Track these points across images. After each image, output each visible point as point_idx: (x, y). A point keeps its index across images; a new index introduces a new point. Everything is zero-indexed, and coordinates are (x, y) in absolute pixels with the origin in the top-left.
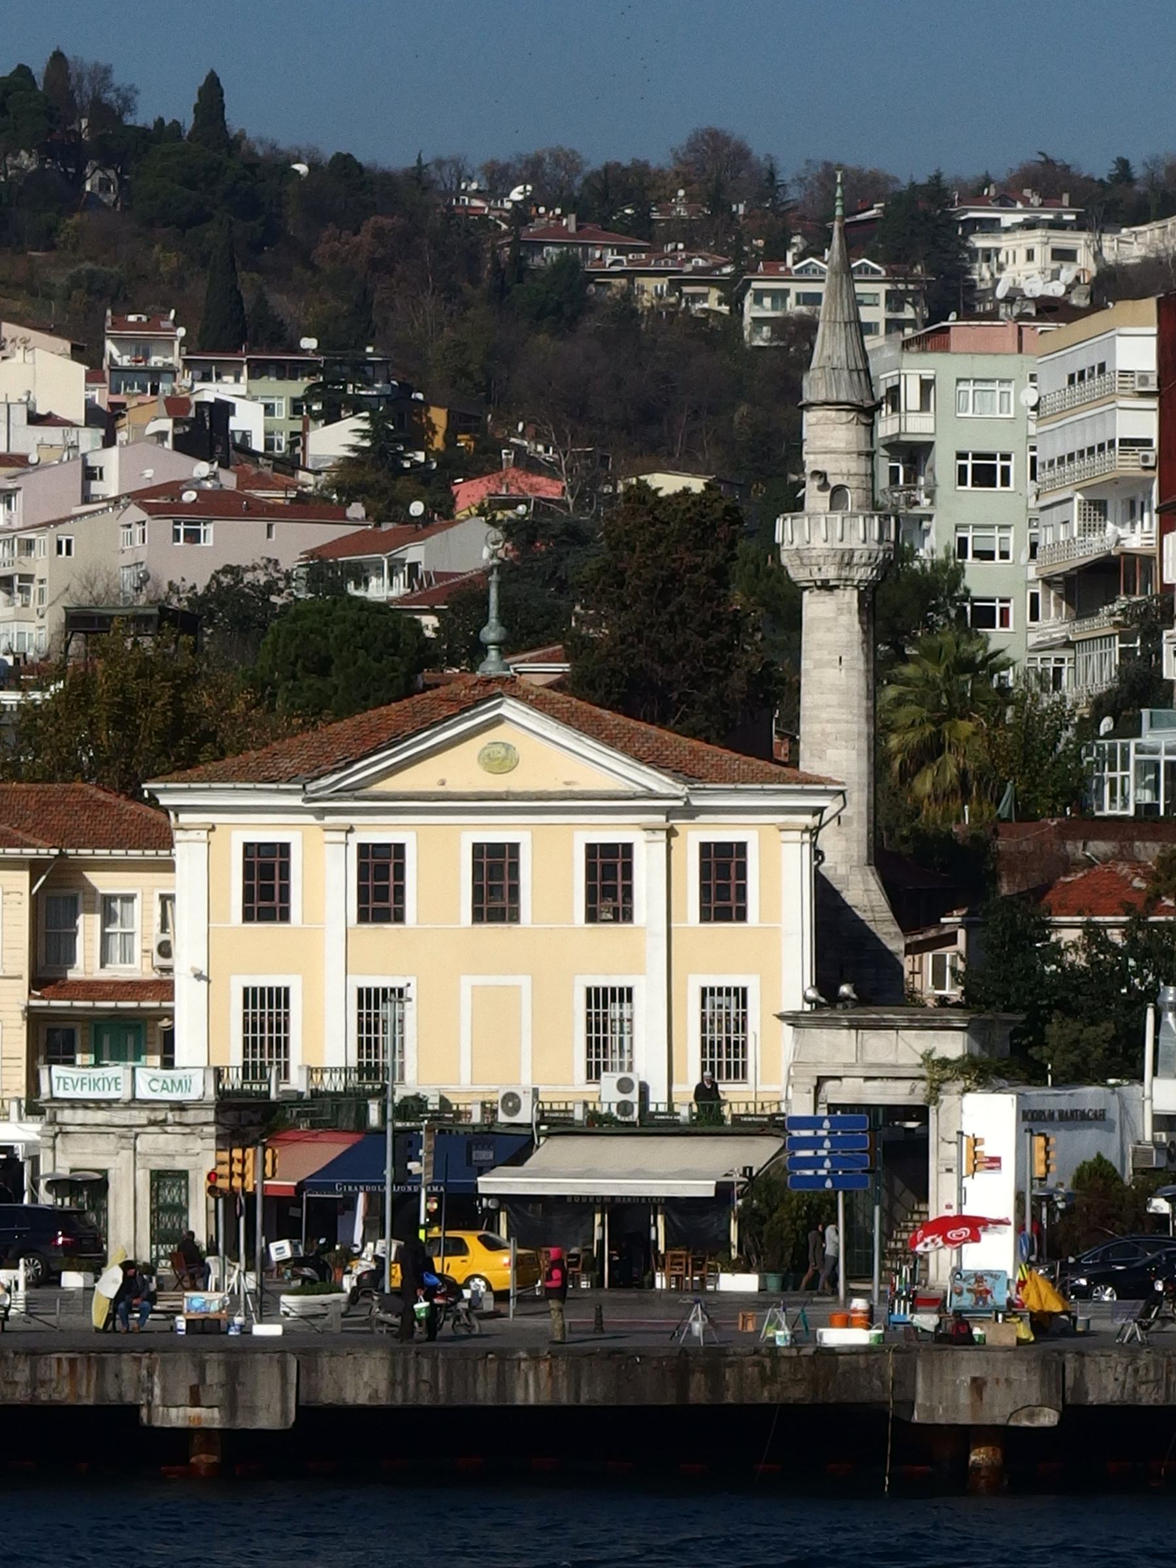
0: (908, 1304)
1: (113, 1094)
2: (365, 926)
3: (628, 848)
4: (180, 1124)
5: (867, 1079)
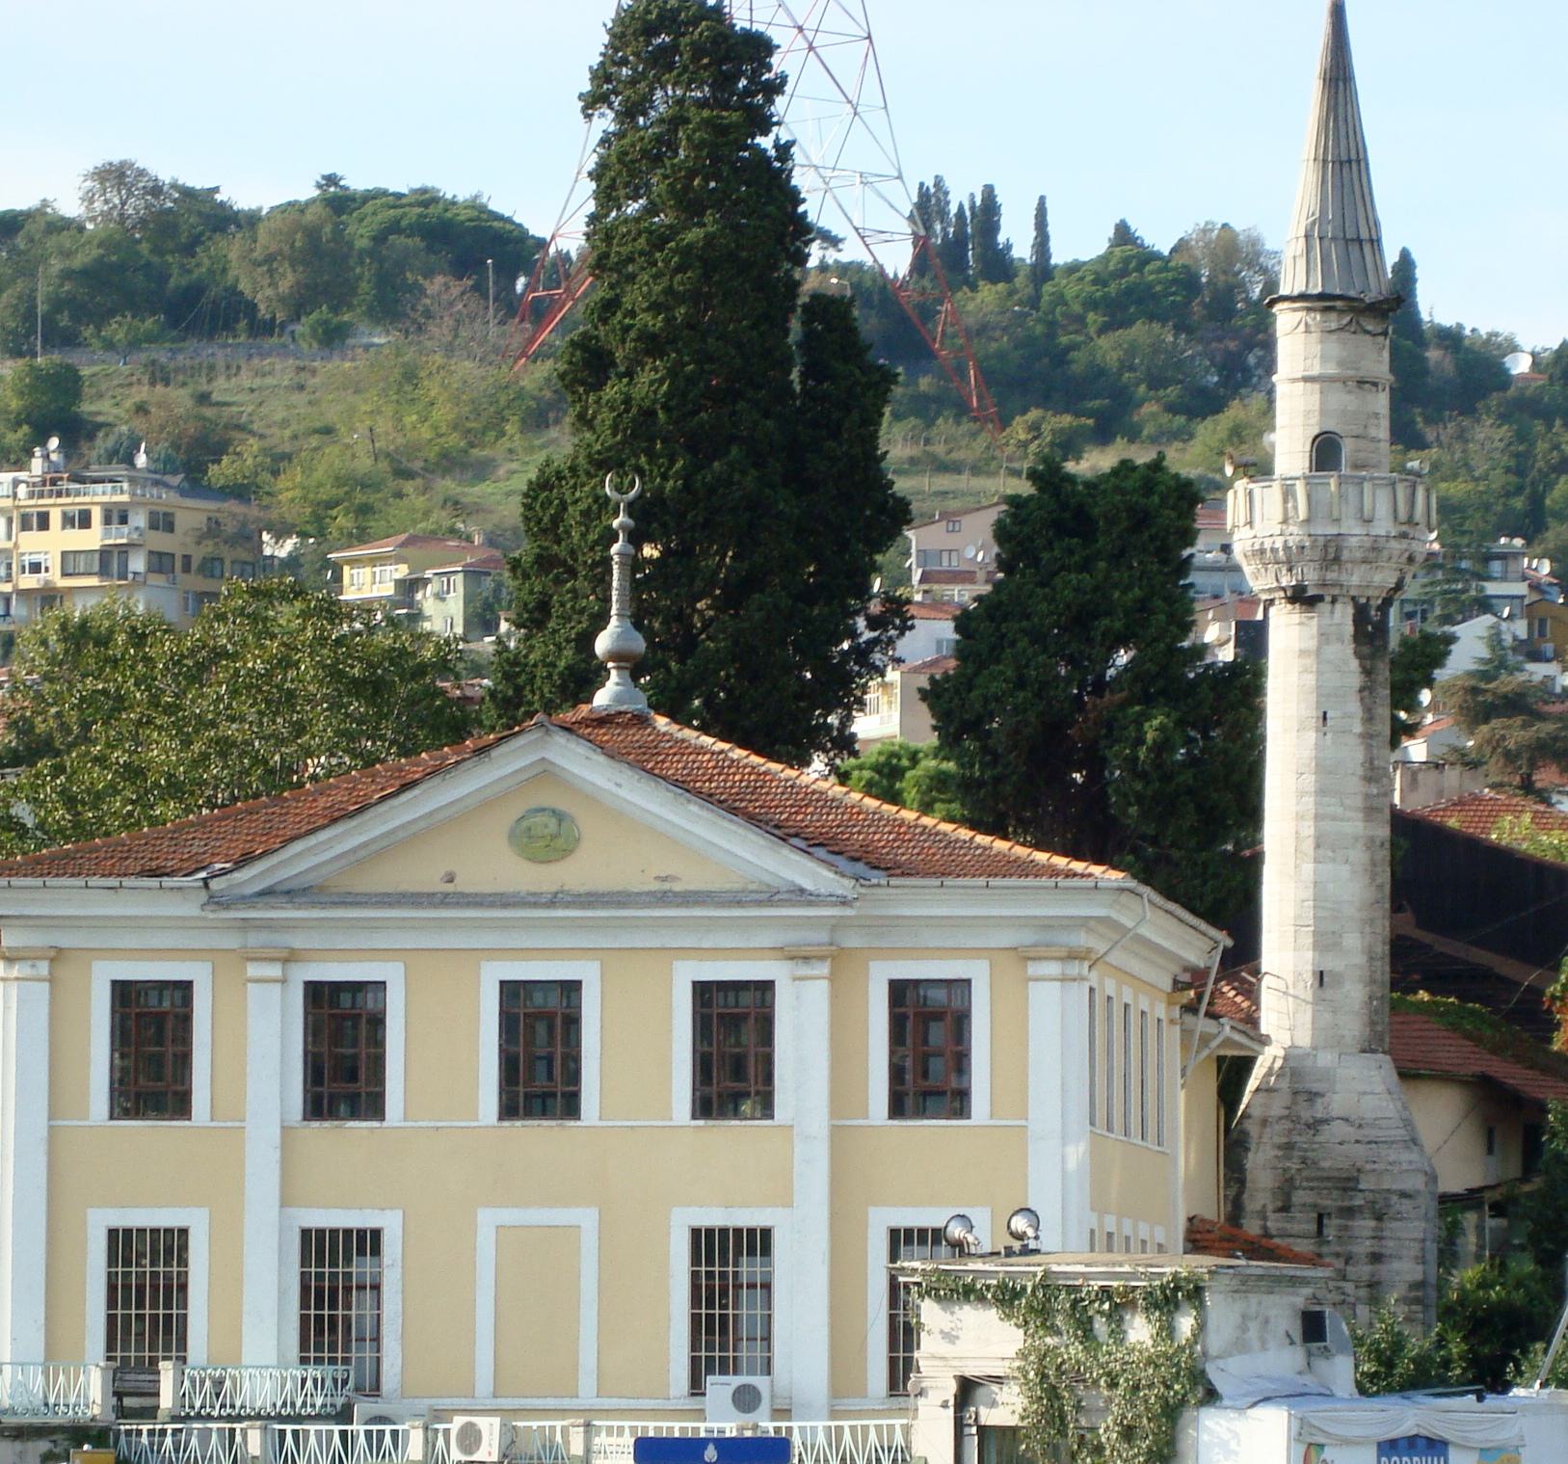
2: (315, 1124)
3: (766, 987)
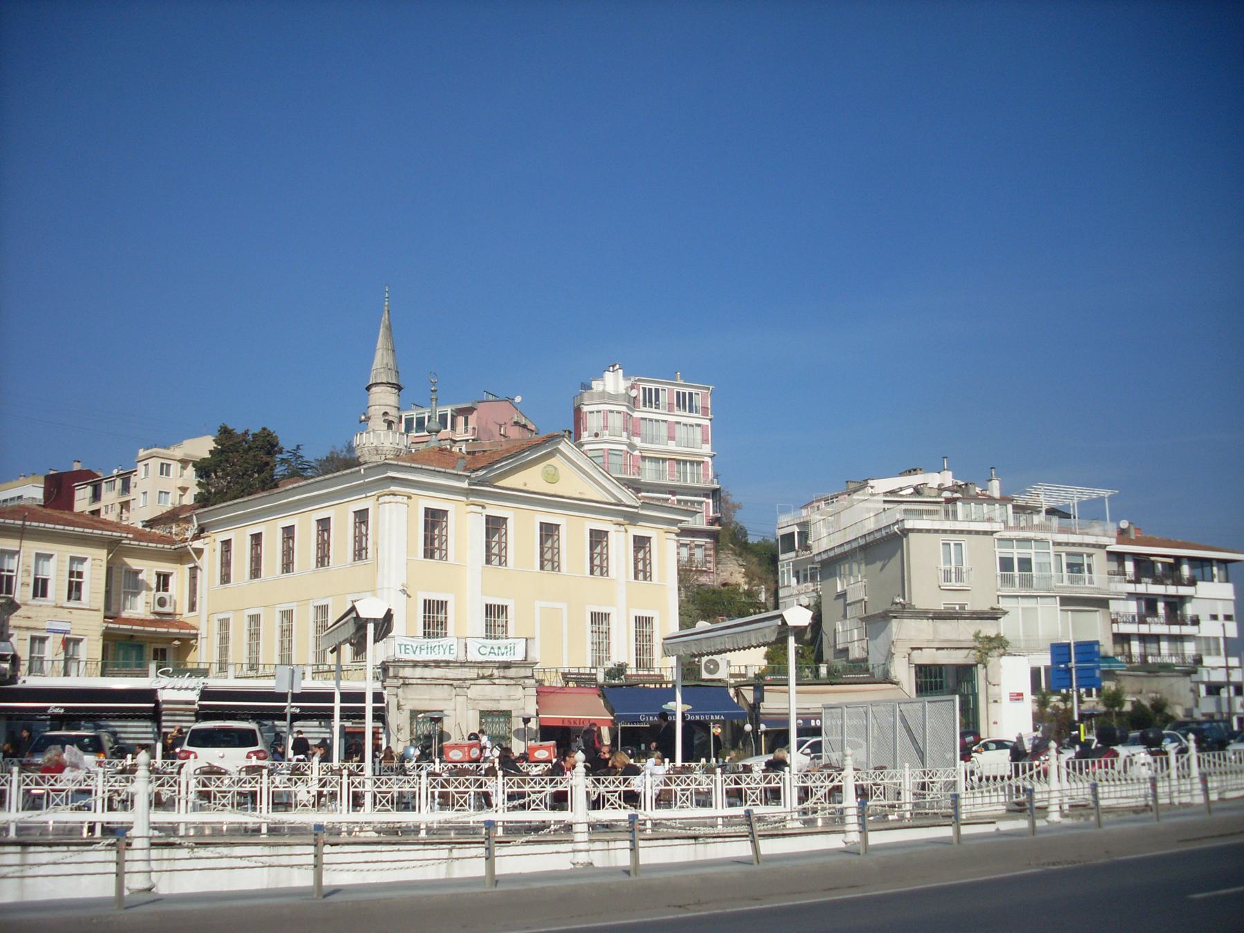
0: (327, 849)
1: (447, 657)
4: (504, 678)
5: (938, 649)
